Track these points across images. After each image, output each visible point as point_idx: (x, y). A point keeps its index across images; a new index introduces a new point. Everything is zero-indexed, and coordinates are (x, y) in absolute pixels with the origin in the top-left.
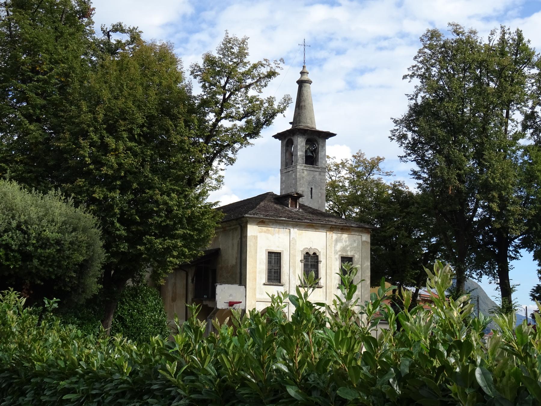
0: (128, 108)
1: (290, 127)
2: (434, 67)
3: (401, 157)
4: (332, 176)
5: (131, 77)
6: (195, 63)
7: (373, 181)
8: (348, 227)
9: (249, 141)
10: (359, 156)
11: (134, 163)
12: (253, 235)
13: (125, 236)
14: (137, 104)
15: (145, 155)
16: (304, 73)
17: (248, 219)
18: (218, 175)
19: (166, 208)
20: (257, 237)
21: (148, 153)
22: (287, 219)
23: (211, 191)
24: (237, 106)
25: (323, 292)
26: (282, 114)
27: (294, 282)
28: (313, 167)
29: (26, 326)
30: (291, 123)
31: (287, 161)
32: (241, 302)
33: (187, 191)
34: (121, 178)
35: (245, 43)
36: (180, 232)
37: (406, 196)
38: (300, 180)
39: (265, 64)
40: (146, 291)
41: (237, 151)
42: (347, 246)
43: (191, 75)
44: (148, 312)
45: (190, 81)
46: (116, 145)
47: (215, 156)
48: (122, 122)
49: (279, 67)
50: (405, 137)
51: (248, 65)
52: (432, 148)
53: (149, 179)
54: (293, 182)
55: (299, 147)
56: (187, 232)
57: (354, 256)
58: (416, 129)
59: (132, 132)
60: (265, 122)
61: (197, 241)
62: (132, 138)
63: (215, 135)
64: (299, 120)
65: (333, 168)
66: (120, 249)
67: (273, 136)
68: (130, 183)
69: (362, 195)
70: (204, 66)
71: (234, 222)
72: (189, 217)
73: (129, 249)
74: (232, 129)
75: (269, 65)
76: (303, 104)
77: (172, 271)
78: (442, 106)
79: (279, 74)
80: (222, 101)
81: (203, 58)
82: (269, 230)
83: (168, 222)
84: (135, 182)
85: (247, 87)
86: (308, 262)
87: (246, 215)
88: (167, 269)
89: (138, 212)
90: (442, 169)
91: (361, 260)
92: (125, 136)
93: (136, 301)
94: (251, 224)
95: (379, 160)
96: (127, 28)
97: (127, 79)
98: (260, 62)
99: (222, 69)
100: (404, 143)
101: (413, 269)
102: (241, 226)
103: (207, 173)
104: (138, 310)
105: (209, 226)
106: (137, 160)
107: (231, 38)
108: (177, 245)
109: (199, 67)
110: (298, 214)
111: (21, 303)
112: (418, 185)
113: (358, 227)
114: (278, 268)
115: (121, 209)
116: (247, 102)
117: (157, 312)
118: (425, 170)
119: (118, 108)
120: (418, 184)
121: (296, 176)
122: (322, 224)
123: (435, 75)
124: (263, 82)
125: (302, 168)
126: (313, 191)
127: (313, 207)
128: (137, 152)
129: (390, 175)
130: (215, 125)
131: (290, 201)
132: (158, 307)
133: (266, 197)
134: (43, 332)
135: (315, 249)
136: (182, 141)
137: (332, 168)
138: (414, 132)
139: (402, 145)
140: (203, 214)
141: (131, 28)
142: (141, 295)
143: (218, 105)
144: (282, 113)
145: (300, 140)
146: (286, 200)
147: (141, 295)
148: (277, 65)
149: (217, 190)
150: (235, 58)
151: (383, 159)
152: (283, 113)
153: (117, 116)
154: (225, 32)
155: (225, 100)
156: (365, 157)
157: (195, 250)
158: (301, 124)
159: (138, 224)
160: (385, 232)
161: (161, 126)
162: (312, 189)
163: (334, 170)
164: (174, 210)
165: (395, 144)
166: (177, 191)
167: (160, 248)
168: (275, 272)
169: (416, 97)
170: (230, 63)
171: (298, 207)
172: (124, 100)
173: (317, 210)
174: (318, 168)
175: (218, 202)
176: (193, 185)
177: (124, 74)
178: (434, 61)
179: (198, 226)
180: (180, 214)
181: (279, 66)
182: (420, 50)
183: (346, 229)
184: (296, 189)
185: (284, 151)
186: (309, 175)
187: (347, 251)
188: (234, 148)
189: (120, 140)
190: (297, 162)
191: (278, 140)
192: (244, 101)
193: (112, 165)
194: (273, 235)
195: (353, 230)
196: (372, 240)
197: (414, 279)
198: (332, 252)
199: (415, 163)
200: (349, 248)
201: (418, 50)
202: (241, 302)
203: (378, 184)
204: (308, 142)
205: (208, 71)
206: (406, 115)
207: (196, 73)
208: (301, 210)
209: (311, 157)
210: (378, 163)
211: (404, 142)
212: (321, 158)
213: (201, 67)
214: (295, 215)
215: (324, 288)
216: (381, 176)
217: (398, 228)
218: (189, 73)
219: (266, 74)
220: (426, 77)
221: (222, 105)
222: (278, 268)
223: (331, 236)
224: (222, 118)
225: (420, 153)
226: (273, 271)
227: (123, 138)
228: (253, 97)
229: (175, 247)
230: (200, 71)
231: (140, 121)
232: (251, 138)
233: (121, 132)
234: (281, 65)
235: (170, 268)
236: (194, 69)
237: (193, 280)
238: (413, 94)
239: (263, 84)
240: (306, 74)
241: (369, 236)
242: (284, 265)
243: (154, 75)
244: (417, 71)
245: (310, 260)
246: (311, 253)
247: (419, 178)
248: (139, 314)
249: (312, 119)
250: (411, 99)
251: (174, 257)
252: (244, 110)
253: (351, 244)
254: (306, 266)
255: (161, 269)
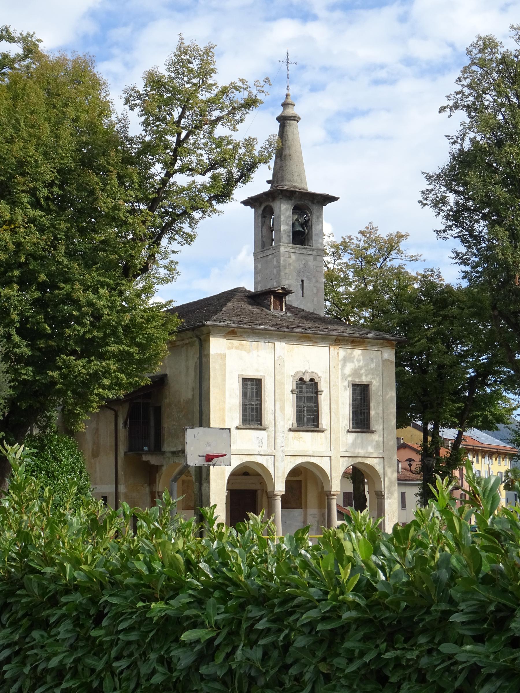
0: (29, 156)
1: (267, 188)
2: (488, 94)
3: (438, 232)
4: (329, 263)
5: (30, 109)
6: (132, 86)
7: (391, 270)
8: (361, 338)
9: (215, 207)
10: (370, 232)
11: (41, 242)
12: (219, 352)
13: (29, 356)
14: (41, 150)
15: (56, 229)
16: (288, 104)
17: (211, 328)
18: (168, 260)
19: (92, 312)
20: (224, 355)
21: (62, 227)
22: (270, 328)
23: (160, 285)
24: (199, 152)
25: (326, 438)
26: (266, 165)
27: (282, 423)
28: (304, 248)
29: (25, 497)
30: (269, 182)
31: (264, 239)
32: (225, 455)
33: (123, 284)
34: (20, 265)
35: (210, 54)
36: (114, 348)
37: (442, 292)
38: (286, 268)
39: (240, 87)
40: (58, 442)
41: (196, 223)
42: (361, 368)
43: (125, 104)
44: (62, 474)
45: (125, 114)
46: (11, 214)
47: (164, 230)
48: (19, 179)
49: (263, 92)
50: (443, 200)
51: (214, 88)
52: (485, 217)
53: (64, 267)
54: (275, 271)
55: (282, 218)
56: (124, 349)
57: (371, 382)
58: (461, 189)
59: (36, 194)
60: (241, 177)
61: (140, 362)
62: (36, 204)
63: (165, 198)
64: (282, 177)
65: (330, 250)
66: (21, 377)
67: (241, 202)
68: (34, 274)
69: (375, 291)
70: (146, 90)
71: (189, 334)
72: (127, 325)
73: (34, 376)
74: (189, 188)
75: (247, 88)
76: (286, 152)
77: (98, 410)
78: (503, 152)
79: (262, 103)
80: (174, 145)
81: (143, 78)
82: (243, 345)
83: (95, 333)
84: (42, 272)
85: (214, 123)
86: (303, 392)
87: (208, 322)
88: (89, 407)
89: (48, 319)
90: (504, 250)
91: (381, 389)
92: (26, 200)
93: (43, 457)
94: (215, 336)
95: (400, 237)
96: (18, 35)
97: (25, 111)
98: (234, 83)
99: (175, 94)
100: (442, 210)
101: (454, 402)
102: (200, 339)
103: (152, 257)
104: (46, 471)
105: (158, 338)
106: (44, 238)
107: (188, 47)
108: (110, 369)
109: (138, 92)
110: (285, 320)
111: (16, 454)
112: (463, 274)
113: (376, 339)
114: (258, 402)
115: (21, 314)
116: (214, 146)
117: (75, 473)
118: (475, 251)
119: (13, 156)
120: (463, 272)
121: (279, 262)
122: (322, 335)
123: (489, 105)
124: (237, 115)
125: (289, 249)
126: (305, 284)
127: (307, 310)
128: (45, 225)
129: (416, 260)
130: (164, 182)
131: (272, 301)
132: (77, 466)
133: (234, 295)
134: (48, 507)
135: (312, 372)
136: (115, 208)
137: (328, 251)
138: (457, 192)
139: (439, 213)
140: (148, 321)
141: (25, 34)
142: (50, 448)
143: (168, 151)
144: (266, 163)
145: (285, 207)
146: (266, 299)
147: (50, 448)
148: (259, 88)
149: (169, 283)
150: (194, 78)
151: (406, 236)
152: (268, 164)
153: (12, 169)
154: (179, 37)
155: (179, 143)
156: (378, 233)
157: (137, 376)
158: (284, 183)
159: (49, 337)
160: (412, 345)
161: (81, 185)
162: (303, 281)
163: (331, 253)
164: (104, 314)
165: (430, 211)
166: (108, 285)
167: (84, 374)
168: (253, 409)
169: (463, 140)
170: (188, 86)
171: (284, 309)
172: (22, 144)
173: (313, 313)
174: (312, 250)
175: (170, 302)
176: (131, 275)
177: (20, 103)
178: (486, 85)
179: (140, 339)
180: (114, 321)
181: (262, 89)
182: (465, 68)
183: (359, 342)
184: (279, 282)
185: (260, 225)
186: (298, 260)
187: (360, 376)
188: (192, 219)
189: (17, 206)
190: (279, 240)
191: (249, 207)
192: (209, 144)
193: (5, 246)
194: (249, 352)
195: (369, 342)
196: (398, 357)
197: (454, 417)
198: (338, 378)
199: (458, 240)
200: (363, 371)
201: (462, 69)
202: (225, 455)
203: (399, 273)
204: (297, 209)
205: (154, 98)
206: (446, 167)
207: (134, 102)
208: (288, 314)
209: (301, 233)
210: (398, 242)
211: (443, 208)
212: (317, 235)
213: (141, 92)
214: (281, 322)
215: (327, 432)
216: (403, 262)
217: (431, 340)
218: (123, 101)
219: (242, 102)
220: (476, 109)
221: (175, 151)
222: (258, 402)
223: (336, 353)
224: (175, 172)
225: (467, 225)
226: (250, 407)
227: (22, 203)
228: (221, 139)
229: (107, 372)
230: (140, 99)
231: (49, 176)
232: (219, 202)
233: (18, 193)
234: (266, 88)
235: (95, 405)
236: (130, 96)
237: (125, 424)
238: (457, 134)
239: (238, 117)
240: (290, 106)
241: (393, 352)
242: (267, 399)
243: (67, 105)
244: (462, 100)
245: (305, 390)
246: (307, 379)
247: (465, 262)
248: (49, 477)
249: (301, 175)
250: (454, 143)
251: (104, 387)
252: (209, 159)
253: (367, 365)
254: (299, 398)
255: (80, 408)
